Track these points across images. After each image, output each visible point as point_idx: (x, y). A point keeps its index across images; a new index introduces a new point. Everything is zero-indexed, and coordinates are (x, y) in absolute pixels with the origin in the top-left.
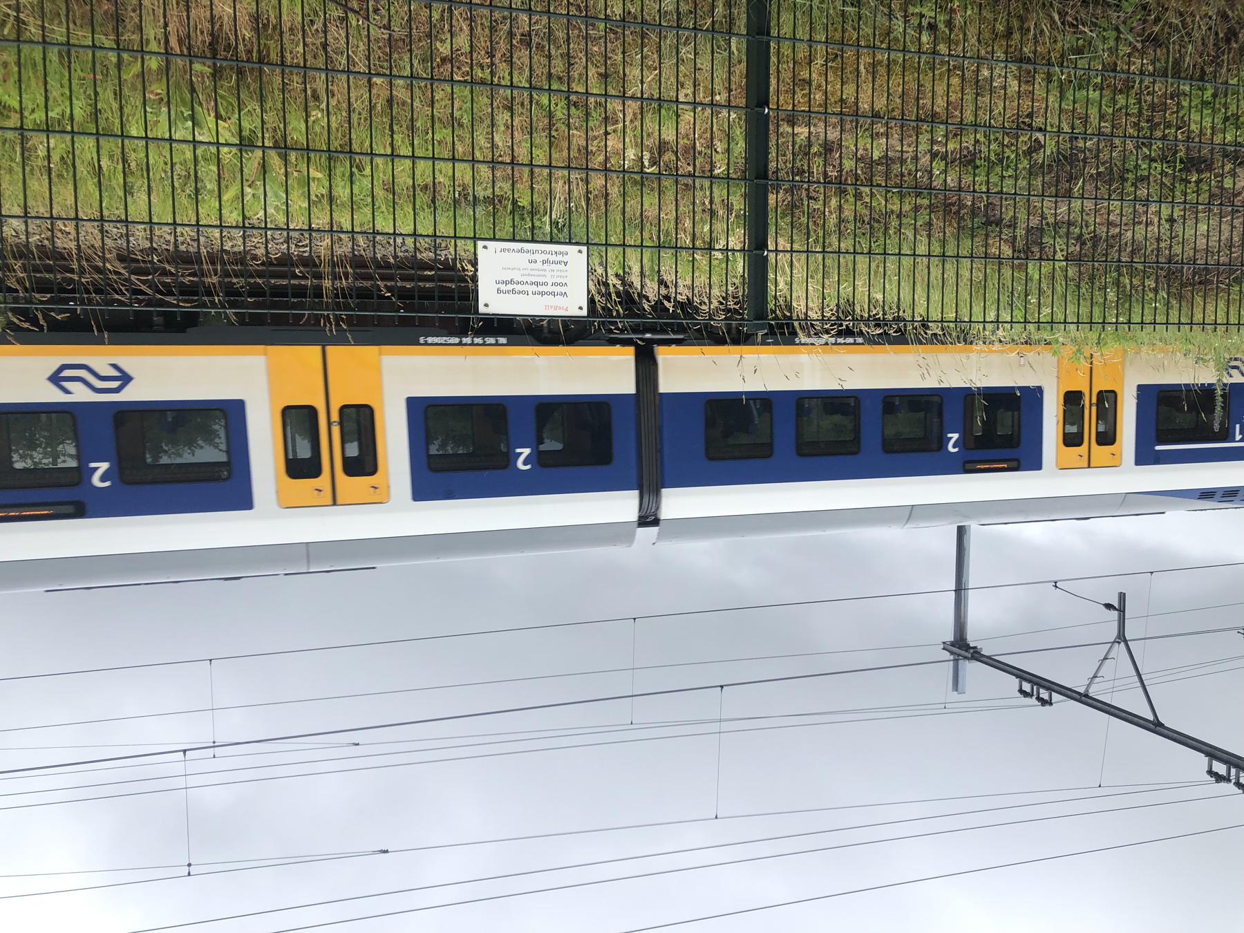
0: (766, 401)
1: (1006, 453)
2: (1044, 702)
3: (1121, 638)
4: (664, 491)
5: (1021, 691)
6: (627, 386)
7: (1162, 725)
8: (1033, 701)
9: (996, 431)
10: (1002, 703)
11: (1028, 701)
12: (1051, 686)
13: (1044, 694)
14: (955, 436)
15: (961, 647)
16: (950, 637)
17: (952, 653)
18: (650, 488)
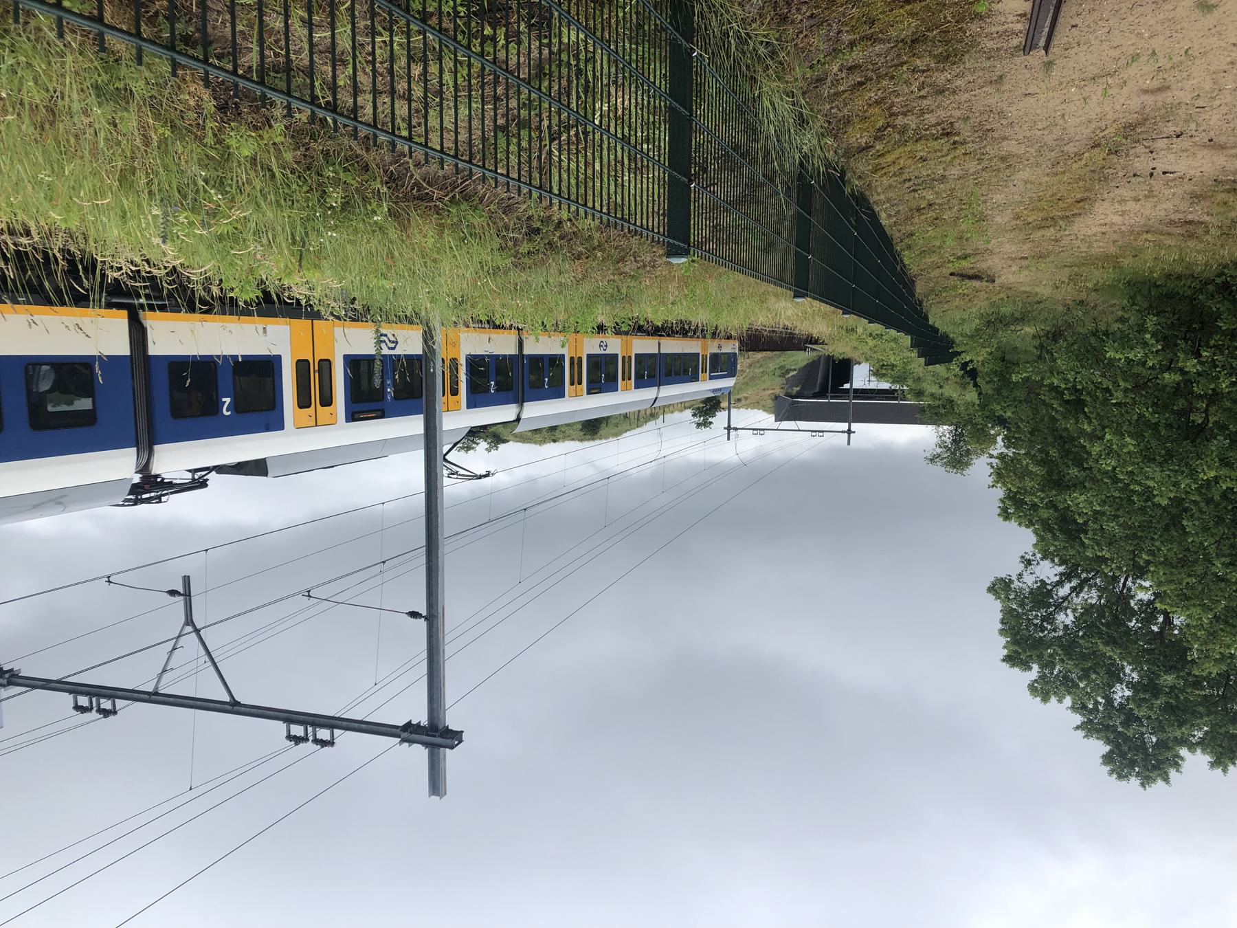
2: (106, 713)
3: (189, 621)
4: (156, 447)
5: (79, 708)
7: (237, 703)
8: (94, 715)
9: (240, 395)
11: (87, 716)
12: (113, 693)
13: (106, 704)
14: (228, 400)
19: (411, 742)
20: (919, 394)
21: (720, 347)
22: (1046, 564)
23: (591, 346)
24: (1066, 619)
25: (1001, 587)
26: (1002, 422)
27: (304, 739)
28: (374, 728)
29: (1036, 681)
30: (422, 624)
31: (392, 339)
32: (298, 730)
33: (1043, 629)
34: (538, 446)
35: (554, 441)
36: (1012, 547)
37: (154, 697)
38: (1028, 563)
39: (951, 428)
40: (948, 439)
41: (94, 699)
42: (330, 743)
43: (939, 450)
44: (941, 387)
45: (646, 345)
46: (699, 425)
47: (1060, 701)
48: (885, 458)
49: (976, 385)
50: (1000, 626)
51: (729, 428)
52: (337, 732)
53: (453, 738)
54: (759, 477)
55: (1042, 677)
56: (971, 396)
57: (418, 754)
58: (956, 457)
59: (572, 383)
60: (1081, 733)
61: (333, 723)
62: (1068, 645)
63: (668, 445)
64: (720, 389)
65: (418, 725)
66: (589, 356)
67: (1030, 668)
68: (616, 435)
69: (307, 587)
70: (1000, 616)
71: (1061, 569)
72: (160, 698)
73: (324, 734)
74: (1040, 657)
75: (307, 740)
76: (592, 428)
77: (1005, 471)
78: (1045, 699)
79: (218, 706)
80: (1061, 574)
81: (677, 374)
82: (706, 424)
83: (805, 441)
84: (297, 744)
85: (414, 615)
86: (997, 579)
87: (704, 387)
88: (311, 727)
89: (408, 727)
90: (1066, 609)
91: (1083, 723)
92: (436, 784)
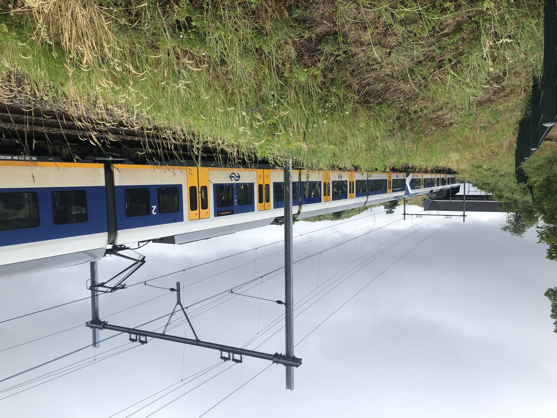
0: (34, 194)
1: (230, 208)
2: (143, 342)
3: (179, 303)
4: (119, 232)
5: (131, 340)
6: (101, 182)
7: (199, 341)
8: (138, 343)
10: (110, 353)
13: (143, 338)
14: (155, 207)
15: (96, 323)
16: (90, 319)
17: (91, 327)
18: (112, 232)
20: (501, 197)
21: (397, 176)
23: (334, 176)
26: (543, 211)
27: (228, 359)
28: (256, 354)
30: (283, 307)
31: (237, 175)
32: (226, 354)
34: (312, 223)
35: (320, 220)
37: (163, 336)
39: (514, 213)
40: (512, 219)
42: (240, 361)
43: (508, 224)
44: (513, 194)
46: (388, 213)
48: (478, 228)
49: (532, 193)
50: (551, 313)
51: (405, 214)
52: (243, 356)
53: (297, 362)
54: (417, 237)
56: (528, 198)
57: (281, 368)
58: (517, 228)
61: (242, 352)
63: (373, 221)
64: (397, 197)
65: (281, 355)
68: (348, 217)
69: (231, 288)
70: (551, 308)
72: (166, 337)
73: (237, 357)
76: (338, 215)
77: (545, 236)
79: (191, 341)
81: (376, 189)
82: (391, 212)
83: (438, 219)
84: (225, 361)
85: (279, 302)
86: (549, 289)
87: (390, 196)
88: (232, 353)
89: (276, 355)
92: (289, 384)
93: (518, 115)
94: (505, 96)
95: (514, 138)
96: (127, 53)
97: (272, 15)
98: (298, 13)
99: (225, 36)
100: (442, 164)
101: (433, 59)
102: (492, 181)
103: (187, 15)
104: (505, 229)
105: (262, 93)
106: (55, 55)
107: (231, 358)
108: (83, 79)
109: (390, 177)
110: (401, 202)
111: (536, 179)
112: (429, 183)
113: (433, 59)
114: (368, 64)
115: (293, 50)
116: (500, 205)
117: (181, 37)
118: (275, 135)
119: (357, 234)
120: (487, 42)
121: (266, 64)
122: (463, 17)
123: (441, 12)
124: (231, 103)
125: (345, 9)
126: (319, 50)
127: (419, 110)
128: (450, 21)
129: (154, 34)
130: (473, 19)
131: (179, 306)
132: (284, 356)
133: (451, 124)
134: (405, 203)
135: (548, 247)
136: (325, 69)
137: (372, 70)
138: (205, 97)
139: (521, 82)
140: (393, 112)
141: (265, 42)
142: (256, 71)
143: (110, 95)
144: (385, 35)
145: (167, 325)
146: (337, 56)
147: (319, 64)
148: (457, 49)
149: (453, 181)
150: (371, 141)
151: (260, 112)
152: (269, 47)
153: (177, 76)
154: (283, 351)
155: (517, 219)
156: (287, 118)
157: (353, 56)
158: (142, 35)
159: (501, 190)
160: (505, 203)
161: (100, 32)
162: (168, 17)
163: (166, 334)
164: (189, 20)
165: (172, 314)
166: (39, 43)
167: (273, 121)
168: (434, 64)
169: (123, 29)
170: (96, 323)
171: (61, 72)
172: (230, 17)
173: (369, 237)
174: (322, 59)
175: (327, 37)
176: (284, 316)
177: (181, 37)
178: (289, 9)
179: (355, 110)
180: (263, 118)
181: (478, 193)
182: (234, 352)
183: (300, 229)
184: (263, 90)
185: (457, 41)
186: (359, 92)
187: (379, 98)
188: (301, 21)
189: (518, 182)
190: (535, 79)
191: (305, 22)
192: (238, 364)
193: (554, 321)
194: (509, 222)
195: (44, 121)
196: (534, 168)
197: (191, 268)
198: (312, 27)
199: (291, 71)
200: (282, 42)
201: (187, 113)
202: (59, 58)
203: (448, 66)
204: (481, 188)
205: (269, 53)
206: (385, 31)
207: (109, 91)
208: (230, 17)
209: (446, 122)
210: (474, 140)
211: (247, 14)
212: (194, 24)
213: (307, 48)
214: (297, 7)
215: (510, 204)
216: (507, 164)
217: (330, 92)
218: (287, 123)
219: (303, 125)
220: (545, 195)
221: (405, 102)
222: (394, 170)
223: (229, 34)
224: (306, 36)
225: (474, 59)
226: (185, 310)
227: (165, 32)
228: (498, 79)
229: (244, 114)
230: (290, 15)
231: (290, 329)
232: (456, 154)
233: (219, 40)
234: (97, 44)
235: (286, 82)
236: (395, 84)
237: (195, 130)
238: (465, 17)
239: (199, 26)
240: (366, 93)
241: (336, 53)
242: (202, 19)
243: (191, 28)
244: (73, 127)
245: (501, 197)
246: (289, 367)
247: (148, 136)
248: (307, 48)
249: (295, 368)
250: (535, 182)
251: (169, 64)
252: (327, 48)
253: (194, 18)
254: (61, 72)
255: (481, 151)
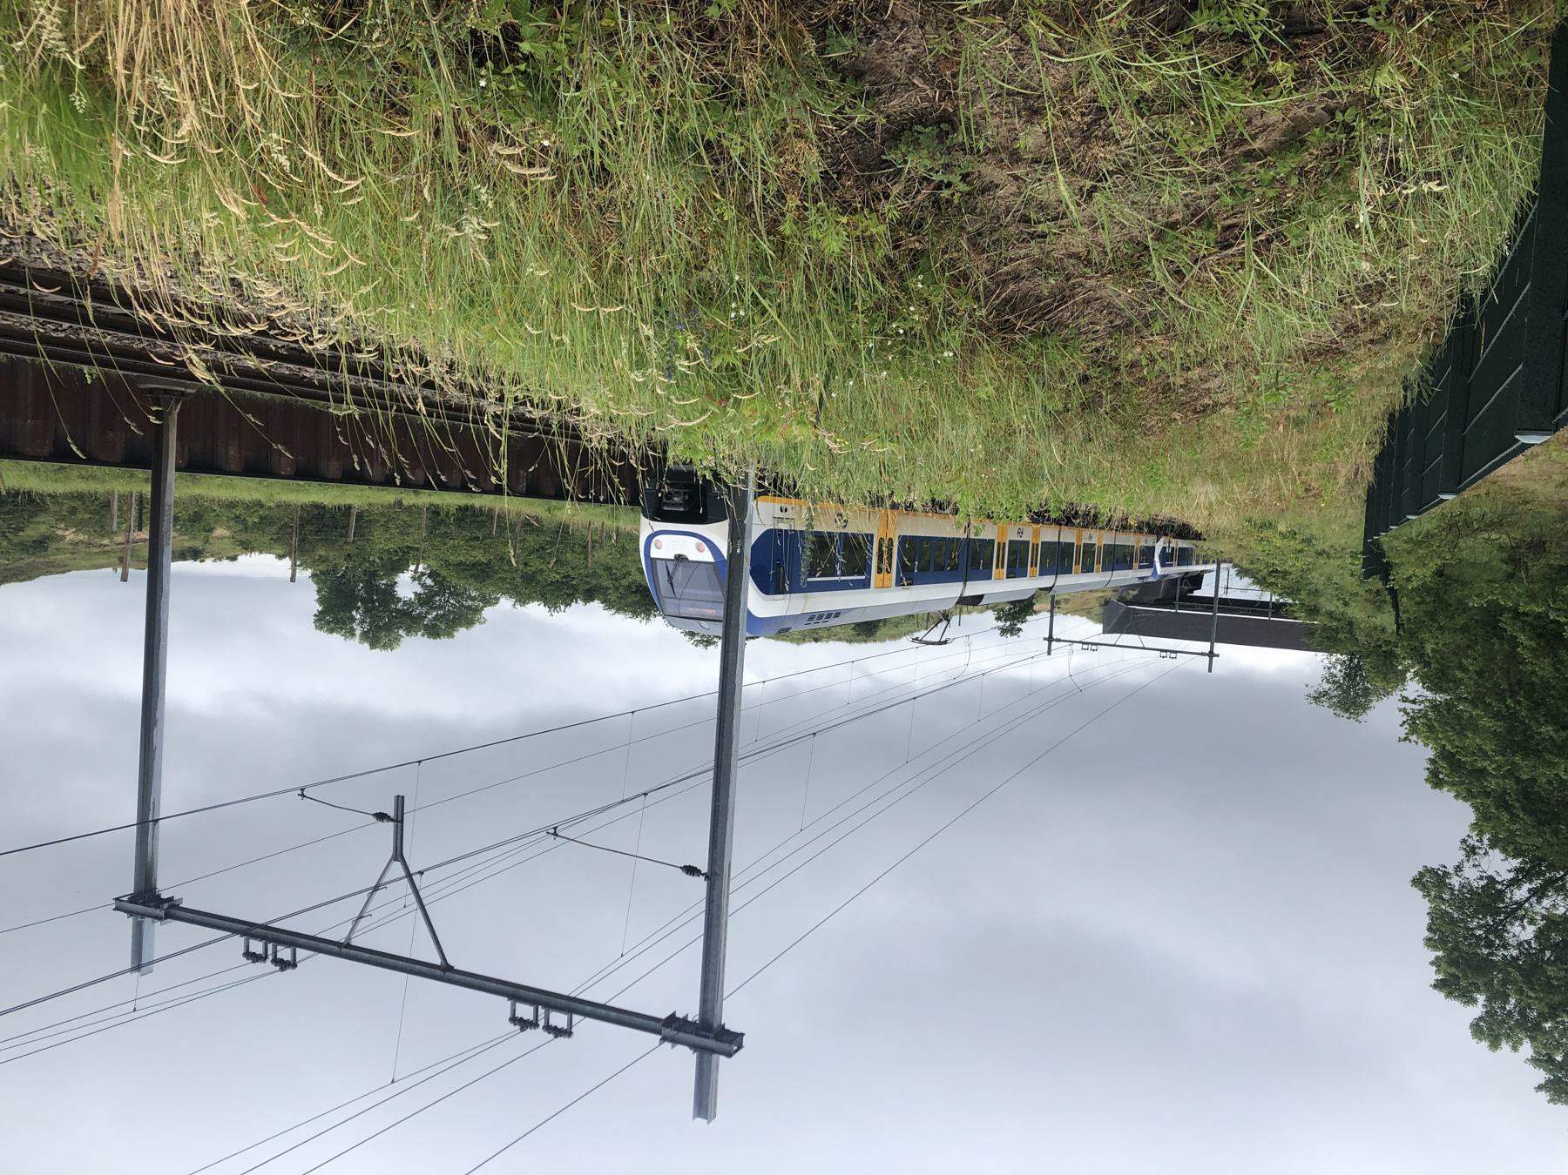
2: (283, 965)
3: (398, 855)
5: (249, 955)
7: (449, 968)
8: (268, 966)
13: (285, 953)
15: (147, 901)
16: (129, 888)
17: (131, 913)
19: (675, 1041)
20: (1313, 611)
22: (1496, 854)
24: (1522, 932)
25: (1431, 881)
26: (1419, 655)
27: (533, 1024)
28: (613, 1014)
29: (1481, 1018)
30: (700, 884)
32: (525, 1011)
33: (1490, 945)
35: (816, 640)
36: (1444, 827)
37: (345, 950)
38: (1471, 851)
39: (1344, 657)
40: (1338, 671)
41: (270, 946)
42: (568, 1033)
43: (1327, 686)
44: (1346, 604)
45: (1049, 534)
46: (1004, 631)
47: (1515, 1049)
48: (1247, 688)
49: (1396, 606)
51: (1050, 639)
52: (576, 1018)
53: (731, 1041)
54: (1074, 699)
55: (1490, 1013)
57: (683, 1059)
58: (1350, 696)
59: (880, 570)
60: (1544, 1096)
62: (1529, 968)
63: (971, 655)
65: (685, 1019)
66: (903, 539)
67: (1474, 1001)
70: (1427, 920)
71: (1516, 863)
73: (559, 1020)
74: (1488, 986)
75: (537, 1025)
76: (867, 630)
77: (1419, 724)
78: (1494, 1045)
79: (426, 969)
80: (1517, 870)
82: (1011, 631)
83: (1139, 660)
84: (522, 1030)
85: (691, 870)
88: (545, 1008)
89: (672, 1020)
90: (1523, 917)
91: (1548, 1082)
92: (704, 1104)
93: (1389, 396)
94: (1372, 341)
95: (1367, 457)
96: (309, 116)
97: (766, 46)
98: (844, 47)
99: (617, 96)
100: (1168, 511)
101: (1206, 221)
102: (1293, 565)
103: (508, 18)
104: (1318, 697)
105: (705, 274)
106: (80, 101)
107: (542, 1023)
108: (161, 184)
109: (1003, 532)
110: (1042, 605)
111: (1413, 572)
112: (1117, 558)
113: (1206, 221)
114: (1026, 220)
115: (814, 156)
116: (1310, 631)
117: (483, 83)
118: (728, 399)
119: (919, 686)
120: (1367, 183)
121: (732, 189)
122: (1311, 109)
123: (1254, 87)
124: (611, 293)
125: (985, 50)
126: (890, 164)
127: (1144, 362)
128: (1274, 116)
129: (397, 68)
130: (1339, 117)
131: (397, 865)
132: (694, 1023)
133: (1216, 406)
134: (1053, 607)
135: (1430, 752)
136: (899, 223)
137: (1032, 236)
138: (536, 271)
139: (1421, 306)
140: (1076, 362)
141: (734, 124)
142: (700, 207)
143: (244, 243)
144: (1086, 139)
145: (360, 917)
146: (939, 187)
147: (885, 206)
148: (1279, 198)
149: (1184, 557)
150: (1001, 438)
151: (694, 330)
152: (749, 139)
153: (455, 200)
154: (691, 1011)
155: (1352, 673)
156: (773, 354)
157: (984, 191)
158: (360, 64)
159: (1316, 593)
160: (1325, 629)
161: (229, 44)
162: (447, 19)
163: (354, 943)
164: (512, 34)
165: (376, 888)
166: (34, 64)
167: (731, 360)
168: (1212, 235)
169: (304, 41)
170: (147, 901)
171: (96, 155)
172: (638, 39)
173: (948, 692)
174: (896, 190)
175: (919, 128)
176: (703, 906)
177: (483, 83)
178: (820, 31)
179: (971, 348)
180: (704, 348)
181: (1254, 594)
182: (550, 1007)
183: (764, 662)
184: (711, 264)
185: (1288, 177)
186: (989, 293)
187: (1040, 318)
188: (851, 72)
189: (1368, 575)
190: (1466, 300)
191: (859, 76)
192: (561, 1039)
193: (1433, 955)
194: (1330, 678)
195: (34, 297)
196: (1410, 540)
197: (446, 755)
198: (879, 93)
199: (801, 220)
200: (786, 130)
201: (473, 312)
202: (92, 112)
203: (1248, 244)
204: (1262, 582)
205: (743, 161)
206: (1089, 125)
207: (241, 227)
208: (638, 39)
209: (1207, 401)
210: (1267, 452)
211: (690, 36)
212: (525, 47)
213: (856, 154)
214: (846, 27)
215: (1337, 630)
216: (1342, 523)
217: (905, 290)
218: (775, 367)
219: (817, 379)
220: (1432, 615)
221: (1110, 336)
222: (1040, 517)
223: (631, 89)
224: (860, 117)
225: (1323, 230)
226: (416, 878)
227: (435, 63)
228: (1371, 291)
229: (647, 331)
230: (821, 51)
231: (717, 948)
232: (1210, 488)
233: (598, 105)
234: (216, 82)
235: (781, 248)
236: (1093, 282)
237: (493, 363)
238: (1319, 108)
239: (540, 54)
240: (1007, 301)
241: (936, 178)
242: (554, 36)
243: (514, 61)
244: (126, 325)
245: (1313, 611)
246: (706, 1056)
247: (352, 370)
248: (856, 154)
249: (722, 1058)
250: (1409, 579)
251: (438, 163)
252: (915, 162)
253: (527, 30)
254: (96, 155)
255: (1278, 482)
